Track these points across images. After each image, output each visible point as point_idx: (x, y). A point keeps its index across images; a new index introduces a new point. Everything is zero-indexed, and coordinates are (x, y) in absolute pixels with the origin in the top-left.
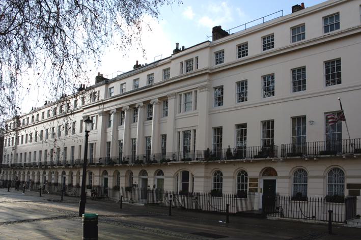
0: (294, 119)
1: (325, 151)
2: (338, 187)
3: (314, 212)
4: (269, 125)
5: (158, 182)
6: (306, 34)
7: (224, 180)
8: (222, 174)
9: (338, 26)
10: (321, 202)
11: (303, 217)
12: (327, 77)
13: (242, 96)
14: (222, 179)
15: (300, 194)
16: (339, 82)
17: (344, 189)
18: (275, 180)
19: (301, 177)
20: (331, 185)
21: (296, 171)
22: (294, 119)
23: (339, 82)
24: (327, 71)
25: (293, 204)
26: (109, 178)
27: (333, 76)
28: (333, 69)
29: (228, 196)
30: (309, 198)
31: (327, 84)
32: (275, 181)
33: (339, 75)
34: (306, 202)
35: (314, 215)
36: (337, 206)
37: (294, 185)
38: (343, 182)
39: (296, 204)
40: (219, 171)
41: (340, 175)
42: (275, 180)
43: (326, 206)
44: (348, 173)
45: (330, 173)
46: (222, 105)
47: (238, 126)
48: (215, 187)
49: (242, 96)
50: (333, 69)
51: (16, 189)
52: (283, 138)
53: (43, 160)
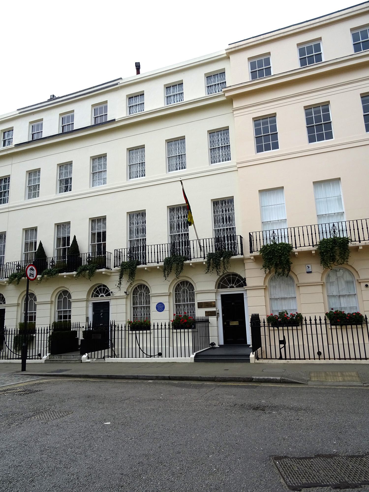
0: (216, 203)
1: (127, 263)
2: (188, 307)
3: (160, 347)
4: (137, 217)
5: (94, 310)
6: (272, 69)
7: (73, 305)
8: (70, 297)
9: (319, 58)
10: (316, 324)
11: (17, 357)
12: (310, 129)
13: (33, 190)
14: (70, 303)
15: (141, 318)
16: (330, 136)
17: (194, 309)
18: (242, 294)
19: (140, 293)
20: (137, 308)
21: (179, 285)
22: (216, 203)
23: (330, 136)
24: (257, 131)
25: (145, 335)
26: (113, 304)
27: (319, 127)
28: (266, 130)
29: (160, 327)
30: (37, 330)
31: (311, 140)
32: (241, 297)
33: (329, 125)
34: (148, 331)
35: (160, 351)
36: (290, 332)
37: (176, 305)
38: (193, 300)
39: (145, 335)
40: (67, 292)
41: (190, 291)
42: (242, 294)
43: (272, 333)
44: (198, 287)
45: (177, 289)
46: (38, 196)
47: (131, 215)
48: (60, 317)
49: (33, 190)
50: (266, 130)
51: (130, 323)
52: (117, 241)
53: (265, 244)
